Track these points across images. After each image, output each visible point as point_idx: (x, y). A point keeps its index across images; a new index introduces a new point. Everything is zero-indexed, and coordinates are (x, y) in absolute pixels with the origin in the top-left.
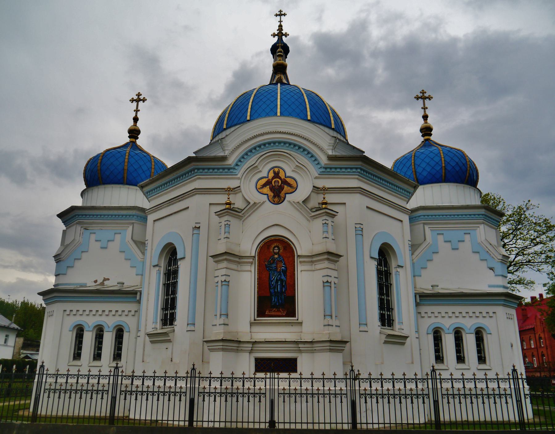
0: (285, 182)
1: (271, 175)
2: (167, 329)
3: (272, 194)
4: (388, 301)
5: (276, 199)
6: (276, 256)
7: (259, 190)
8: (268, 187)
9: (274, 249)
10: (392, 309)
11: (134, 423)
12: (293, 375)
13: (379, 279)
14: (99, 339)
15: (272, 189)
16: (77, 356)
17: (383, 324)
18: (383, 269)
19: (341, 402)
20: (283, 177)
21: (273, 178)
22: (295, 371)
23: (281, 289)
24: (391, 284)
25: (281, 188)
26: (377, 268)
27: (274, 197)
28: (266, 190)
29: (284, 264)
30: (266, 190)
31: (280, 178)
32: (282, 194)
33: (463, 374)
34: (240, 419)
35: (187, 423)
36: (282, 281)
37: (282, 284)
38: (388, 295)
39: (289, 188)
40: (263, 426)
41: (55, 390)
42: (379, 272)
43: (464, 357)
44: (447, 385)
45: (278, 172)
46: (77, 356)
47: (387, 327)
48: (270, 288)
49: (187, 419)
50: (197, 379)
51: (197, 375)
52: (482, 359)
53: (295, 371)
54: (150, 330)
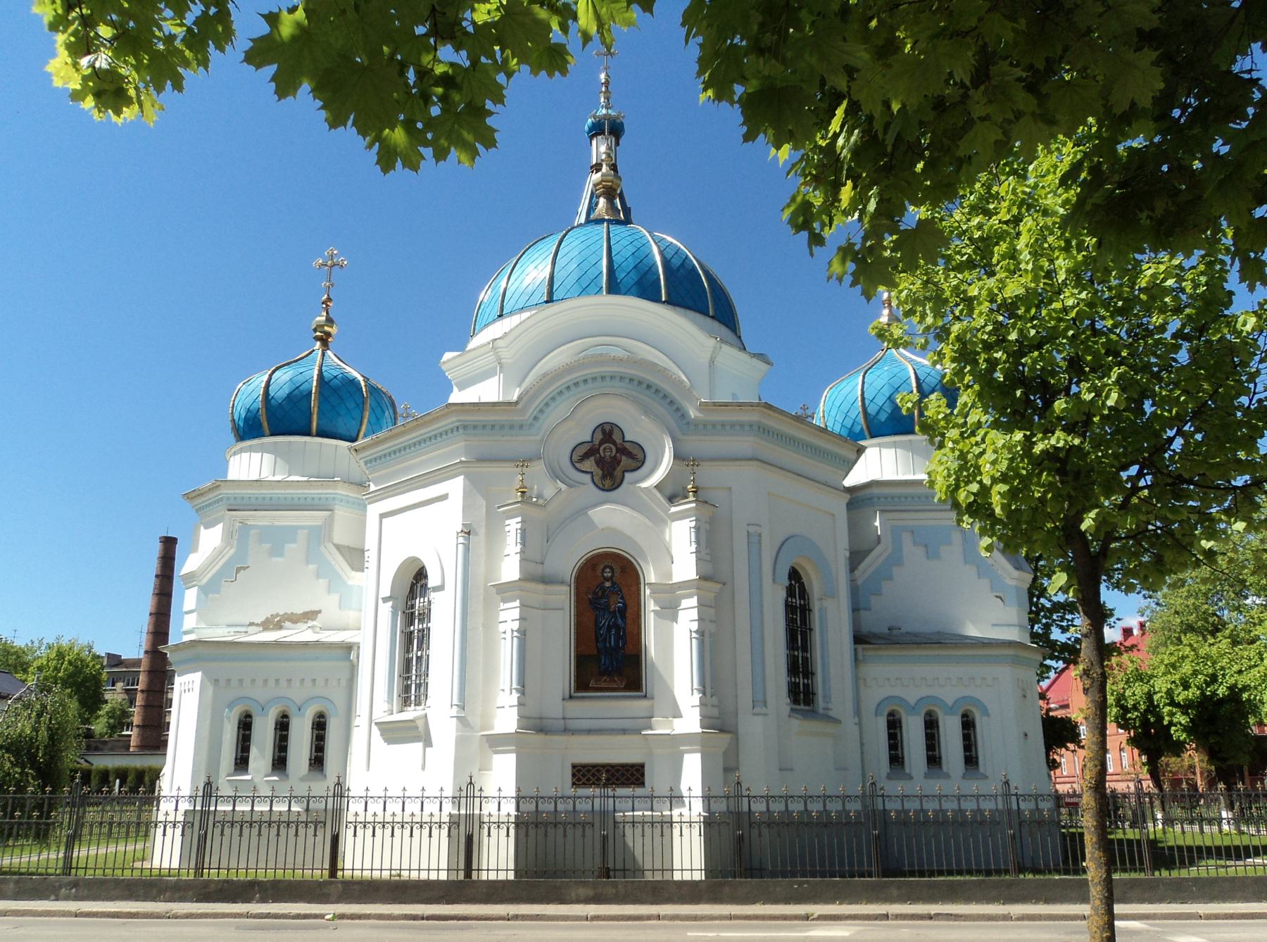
0: (623, 451)
1: (599, 436)
2: (411, 713)
3: (600, 472)
4: (805, 660)
5: (608, 483)
6: (608, 584)
7: (577, 465)
8: (592, 458)
9: (603, 571)
10: (813, 674)
11: (400, 875)
12: (639, 791)
13: (790, 622)
14: (281, 730)
15: (600, 463)
16: (242, 763)
17: (795, 701)
18: (797, 601)
19: (393, 835)
20: (619, 441)
21: (601, 444)
22: (642, 784)
23: (617, 642)
24: (811, 630)
25: (615, 462)
26: (786, 601)
27: (604, 477)
28: (589, 464)
29: (622, 598)
30: (589, 464)
31: (614, 443)
32: (618, 473)
33: (310, 789)
34: (424, 866)
35: (326, 873)
36: (618, 628)
37: (618, 633)
38: (805, 648)
39: (630, 461)
40: (502, 876)
41: (270, 824)
42: (790, 608)
43: (977, 758)
44: (225, 807)
45: (611, 433)
46: (242, 763)
47: (802, 707)
48: (597, 641)
49: (462, 866)
50: (477, 801)
51: (477, 794)
52: (971, 760)
53: (642, 784)
54: (381, 714)
